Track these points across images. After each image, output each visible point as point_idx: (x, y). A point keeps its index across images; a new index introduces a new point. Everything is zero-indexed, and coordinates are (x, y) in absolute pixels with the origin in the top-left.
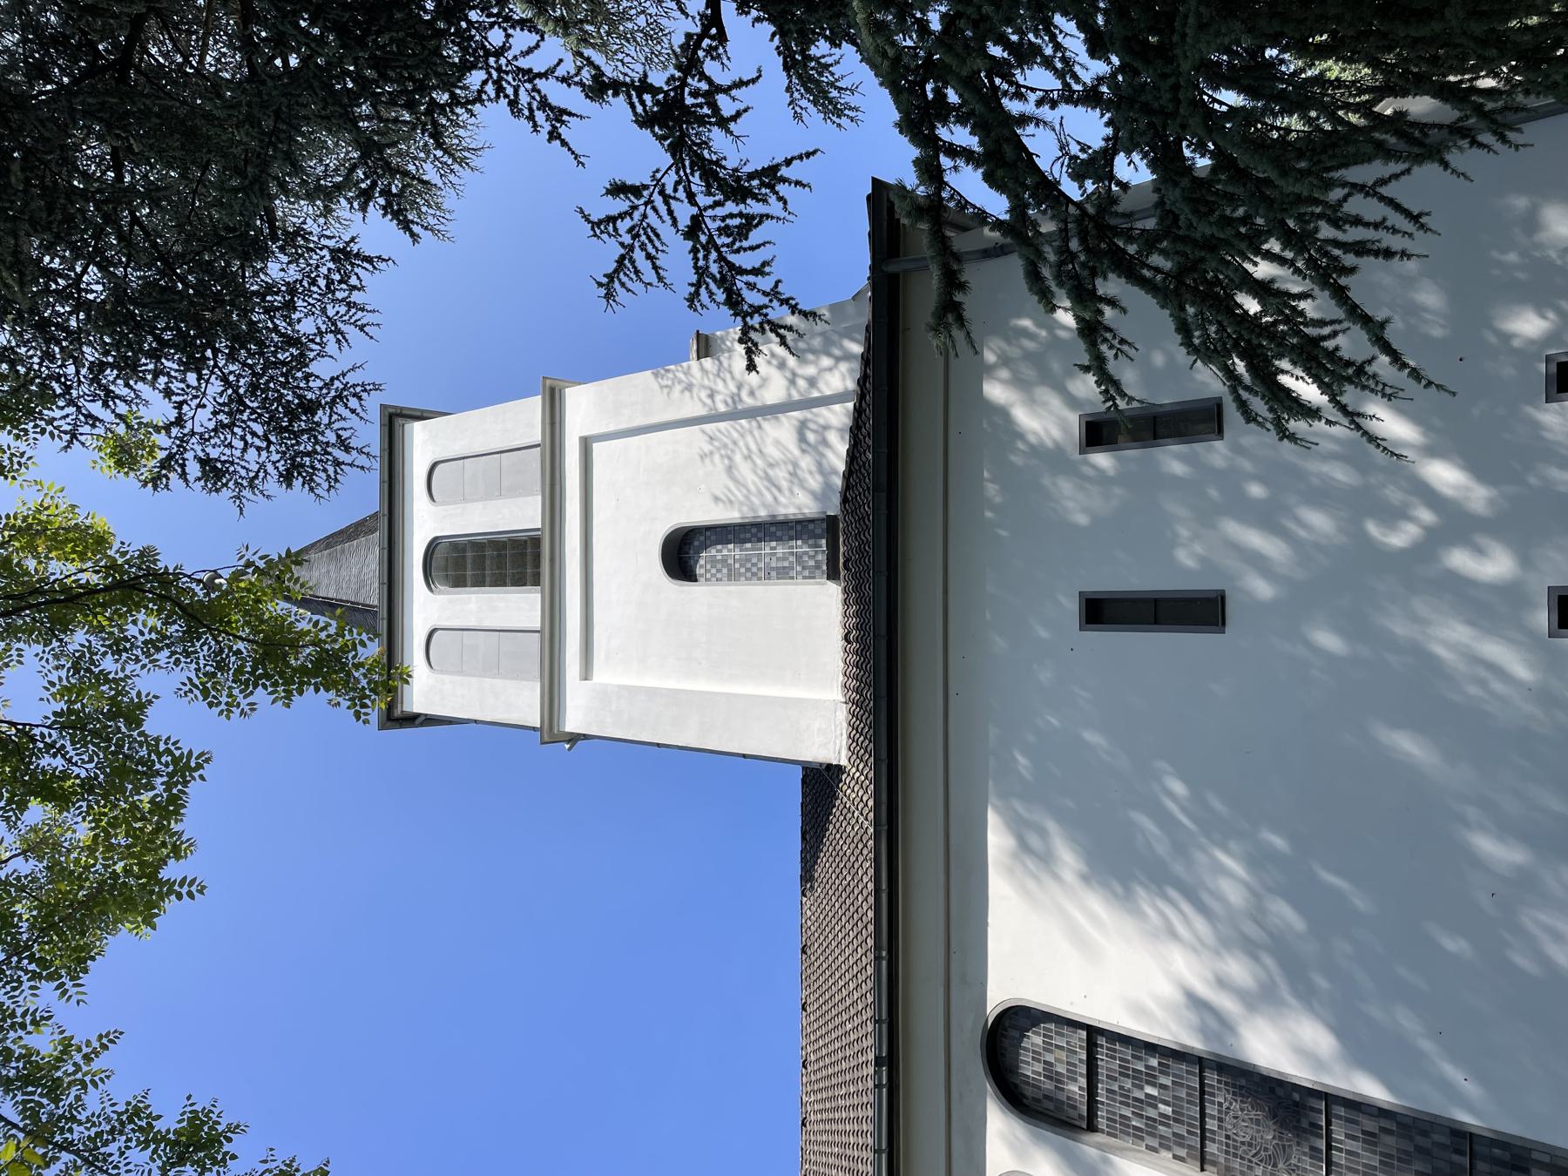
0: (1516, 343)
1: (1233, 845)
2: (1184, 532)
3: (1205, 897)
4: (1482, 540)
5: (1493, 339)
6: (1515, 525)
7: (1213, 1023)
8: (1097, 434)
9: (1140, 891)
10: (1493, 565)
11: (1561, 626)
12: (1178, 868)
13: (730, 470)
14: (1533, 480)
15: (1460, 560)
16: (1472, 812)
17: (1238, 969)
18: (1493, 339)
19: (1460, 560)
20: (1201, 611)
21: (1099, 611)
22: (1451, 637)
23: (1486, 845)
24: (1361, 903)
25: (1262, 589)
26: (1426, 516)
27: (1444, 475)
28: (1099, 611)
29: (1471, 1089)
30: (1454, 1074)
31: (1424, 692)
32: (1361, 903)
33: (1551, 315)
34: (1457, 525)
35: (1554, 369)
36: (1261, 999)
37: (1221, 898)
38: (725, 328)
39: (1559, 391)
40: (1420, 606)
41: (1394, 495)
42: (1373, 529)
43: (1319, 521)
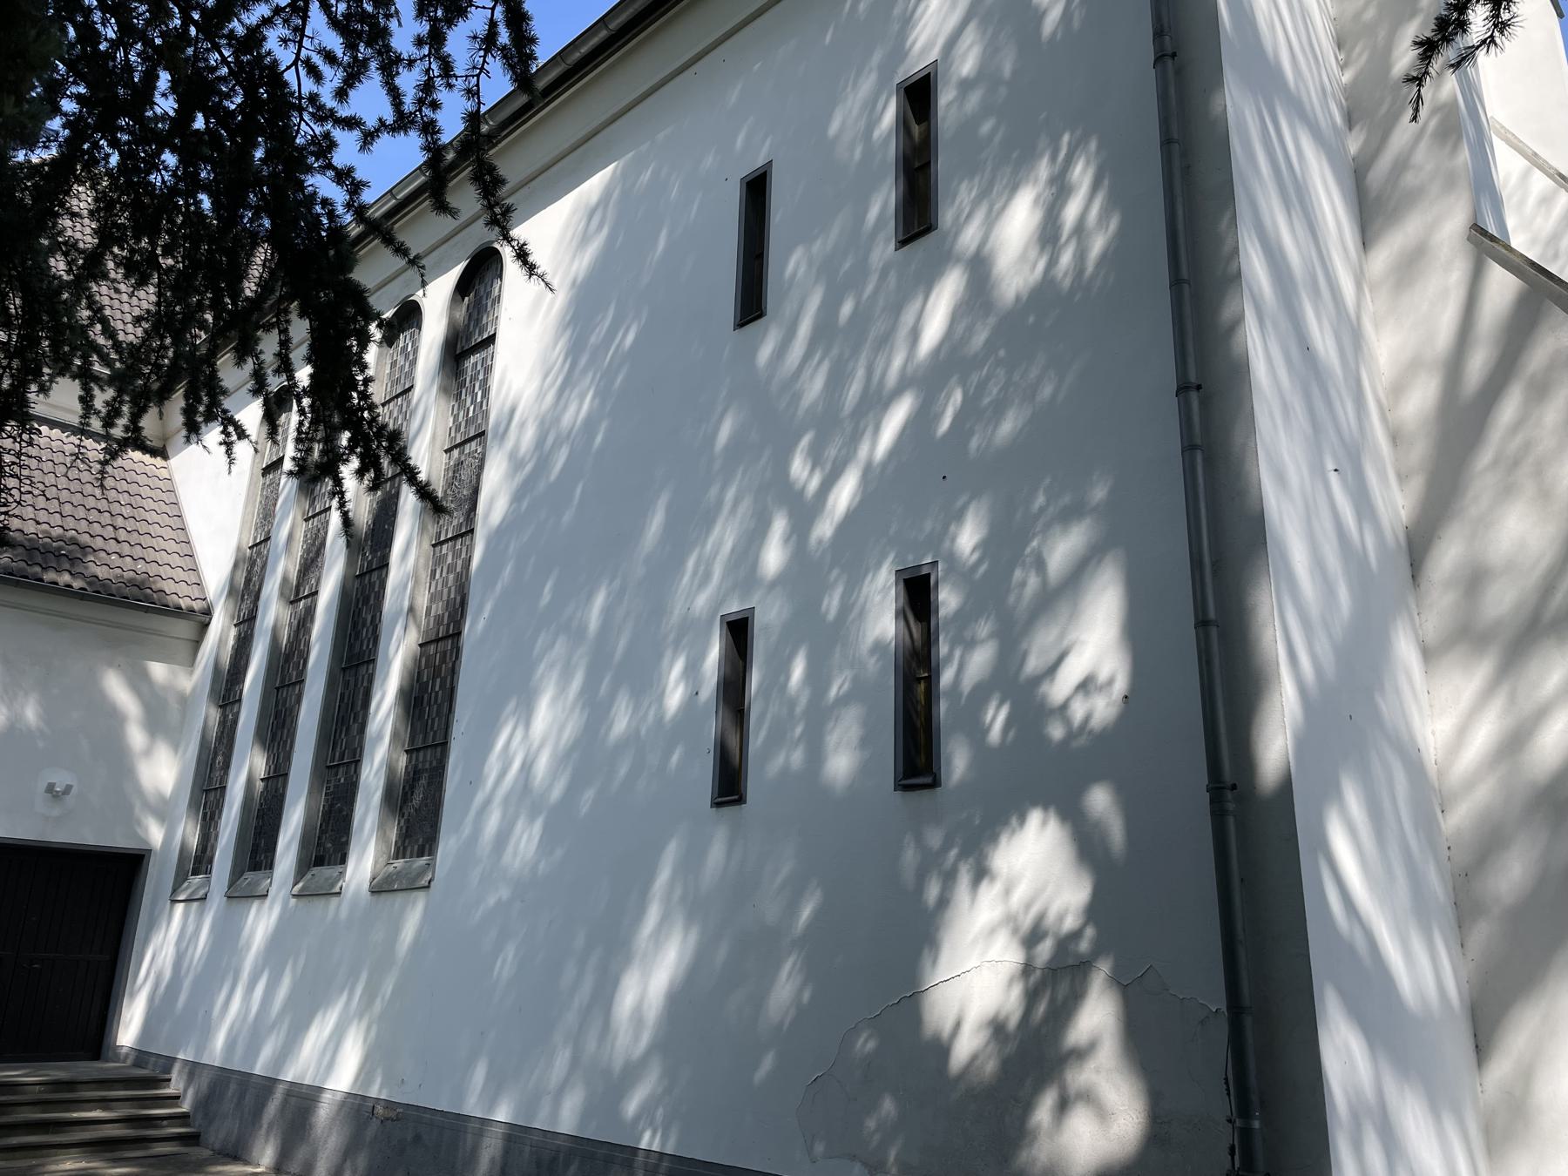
0: (952, 528)
1: (597, 401)
2: (817, 246)
3: (567, 393)
4: (794, 538)
5: (959, 503)
6: (806, 568)
7: (501, 430)
8: (919, 95)
9: (568, 333)
10: (773, 557)
11: (729, 623)
12: (583, 361)
13: (356, 188)
14: (835, 572)
15: (779, 526)
16: (617, 583)
17: (530, 434)
18: (959, 503)
19: (779, 526)
20: (751, 304)
21: (757, 189)
22: (725, 536)
23: (599, 600)
24: (567, 518)
25: (765, 353)
26: (814, 484)
27: (845, 494)
28: (757, 189)
29: (481, 624)
30: (488, 607)
31: (690, 523)
32: (567, 518)
33: (975, 556)
34: (805, 511)
35: (925, 571)
36: (516, 463)
37: (566, 407)
38: (1547, 223)
39: (906, 581)
40: (746, 505)
41: (832, 452)
42: (805, 441)
43: (815, 387)
